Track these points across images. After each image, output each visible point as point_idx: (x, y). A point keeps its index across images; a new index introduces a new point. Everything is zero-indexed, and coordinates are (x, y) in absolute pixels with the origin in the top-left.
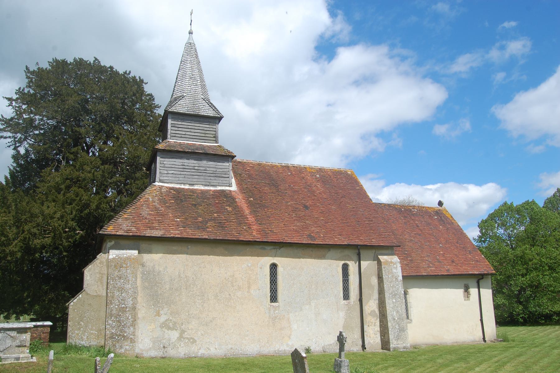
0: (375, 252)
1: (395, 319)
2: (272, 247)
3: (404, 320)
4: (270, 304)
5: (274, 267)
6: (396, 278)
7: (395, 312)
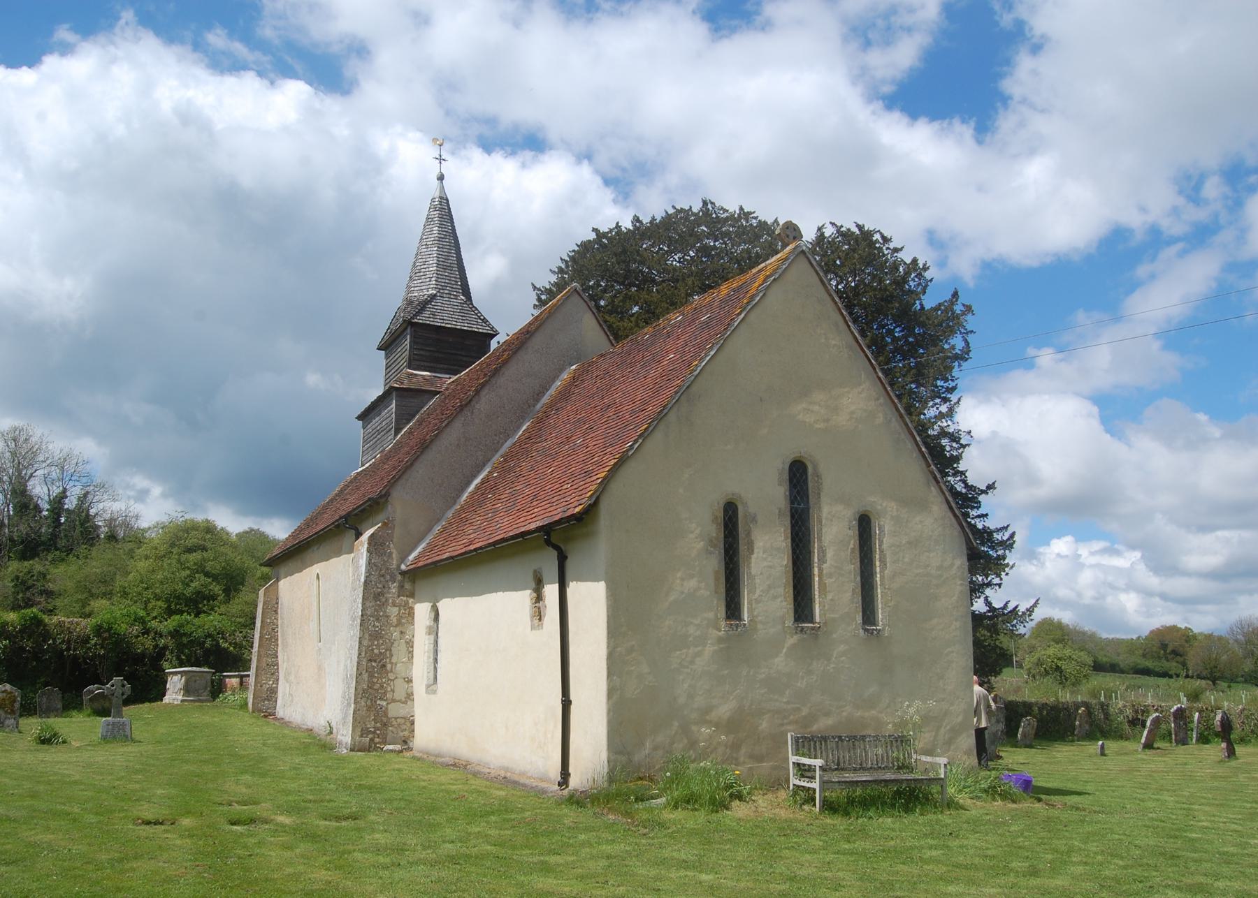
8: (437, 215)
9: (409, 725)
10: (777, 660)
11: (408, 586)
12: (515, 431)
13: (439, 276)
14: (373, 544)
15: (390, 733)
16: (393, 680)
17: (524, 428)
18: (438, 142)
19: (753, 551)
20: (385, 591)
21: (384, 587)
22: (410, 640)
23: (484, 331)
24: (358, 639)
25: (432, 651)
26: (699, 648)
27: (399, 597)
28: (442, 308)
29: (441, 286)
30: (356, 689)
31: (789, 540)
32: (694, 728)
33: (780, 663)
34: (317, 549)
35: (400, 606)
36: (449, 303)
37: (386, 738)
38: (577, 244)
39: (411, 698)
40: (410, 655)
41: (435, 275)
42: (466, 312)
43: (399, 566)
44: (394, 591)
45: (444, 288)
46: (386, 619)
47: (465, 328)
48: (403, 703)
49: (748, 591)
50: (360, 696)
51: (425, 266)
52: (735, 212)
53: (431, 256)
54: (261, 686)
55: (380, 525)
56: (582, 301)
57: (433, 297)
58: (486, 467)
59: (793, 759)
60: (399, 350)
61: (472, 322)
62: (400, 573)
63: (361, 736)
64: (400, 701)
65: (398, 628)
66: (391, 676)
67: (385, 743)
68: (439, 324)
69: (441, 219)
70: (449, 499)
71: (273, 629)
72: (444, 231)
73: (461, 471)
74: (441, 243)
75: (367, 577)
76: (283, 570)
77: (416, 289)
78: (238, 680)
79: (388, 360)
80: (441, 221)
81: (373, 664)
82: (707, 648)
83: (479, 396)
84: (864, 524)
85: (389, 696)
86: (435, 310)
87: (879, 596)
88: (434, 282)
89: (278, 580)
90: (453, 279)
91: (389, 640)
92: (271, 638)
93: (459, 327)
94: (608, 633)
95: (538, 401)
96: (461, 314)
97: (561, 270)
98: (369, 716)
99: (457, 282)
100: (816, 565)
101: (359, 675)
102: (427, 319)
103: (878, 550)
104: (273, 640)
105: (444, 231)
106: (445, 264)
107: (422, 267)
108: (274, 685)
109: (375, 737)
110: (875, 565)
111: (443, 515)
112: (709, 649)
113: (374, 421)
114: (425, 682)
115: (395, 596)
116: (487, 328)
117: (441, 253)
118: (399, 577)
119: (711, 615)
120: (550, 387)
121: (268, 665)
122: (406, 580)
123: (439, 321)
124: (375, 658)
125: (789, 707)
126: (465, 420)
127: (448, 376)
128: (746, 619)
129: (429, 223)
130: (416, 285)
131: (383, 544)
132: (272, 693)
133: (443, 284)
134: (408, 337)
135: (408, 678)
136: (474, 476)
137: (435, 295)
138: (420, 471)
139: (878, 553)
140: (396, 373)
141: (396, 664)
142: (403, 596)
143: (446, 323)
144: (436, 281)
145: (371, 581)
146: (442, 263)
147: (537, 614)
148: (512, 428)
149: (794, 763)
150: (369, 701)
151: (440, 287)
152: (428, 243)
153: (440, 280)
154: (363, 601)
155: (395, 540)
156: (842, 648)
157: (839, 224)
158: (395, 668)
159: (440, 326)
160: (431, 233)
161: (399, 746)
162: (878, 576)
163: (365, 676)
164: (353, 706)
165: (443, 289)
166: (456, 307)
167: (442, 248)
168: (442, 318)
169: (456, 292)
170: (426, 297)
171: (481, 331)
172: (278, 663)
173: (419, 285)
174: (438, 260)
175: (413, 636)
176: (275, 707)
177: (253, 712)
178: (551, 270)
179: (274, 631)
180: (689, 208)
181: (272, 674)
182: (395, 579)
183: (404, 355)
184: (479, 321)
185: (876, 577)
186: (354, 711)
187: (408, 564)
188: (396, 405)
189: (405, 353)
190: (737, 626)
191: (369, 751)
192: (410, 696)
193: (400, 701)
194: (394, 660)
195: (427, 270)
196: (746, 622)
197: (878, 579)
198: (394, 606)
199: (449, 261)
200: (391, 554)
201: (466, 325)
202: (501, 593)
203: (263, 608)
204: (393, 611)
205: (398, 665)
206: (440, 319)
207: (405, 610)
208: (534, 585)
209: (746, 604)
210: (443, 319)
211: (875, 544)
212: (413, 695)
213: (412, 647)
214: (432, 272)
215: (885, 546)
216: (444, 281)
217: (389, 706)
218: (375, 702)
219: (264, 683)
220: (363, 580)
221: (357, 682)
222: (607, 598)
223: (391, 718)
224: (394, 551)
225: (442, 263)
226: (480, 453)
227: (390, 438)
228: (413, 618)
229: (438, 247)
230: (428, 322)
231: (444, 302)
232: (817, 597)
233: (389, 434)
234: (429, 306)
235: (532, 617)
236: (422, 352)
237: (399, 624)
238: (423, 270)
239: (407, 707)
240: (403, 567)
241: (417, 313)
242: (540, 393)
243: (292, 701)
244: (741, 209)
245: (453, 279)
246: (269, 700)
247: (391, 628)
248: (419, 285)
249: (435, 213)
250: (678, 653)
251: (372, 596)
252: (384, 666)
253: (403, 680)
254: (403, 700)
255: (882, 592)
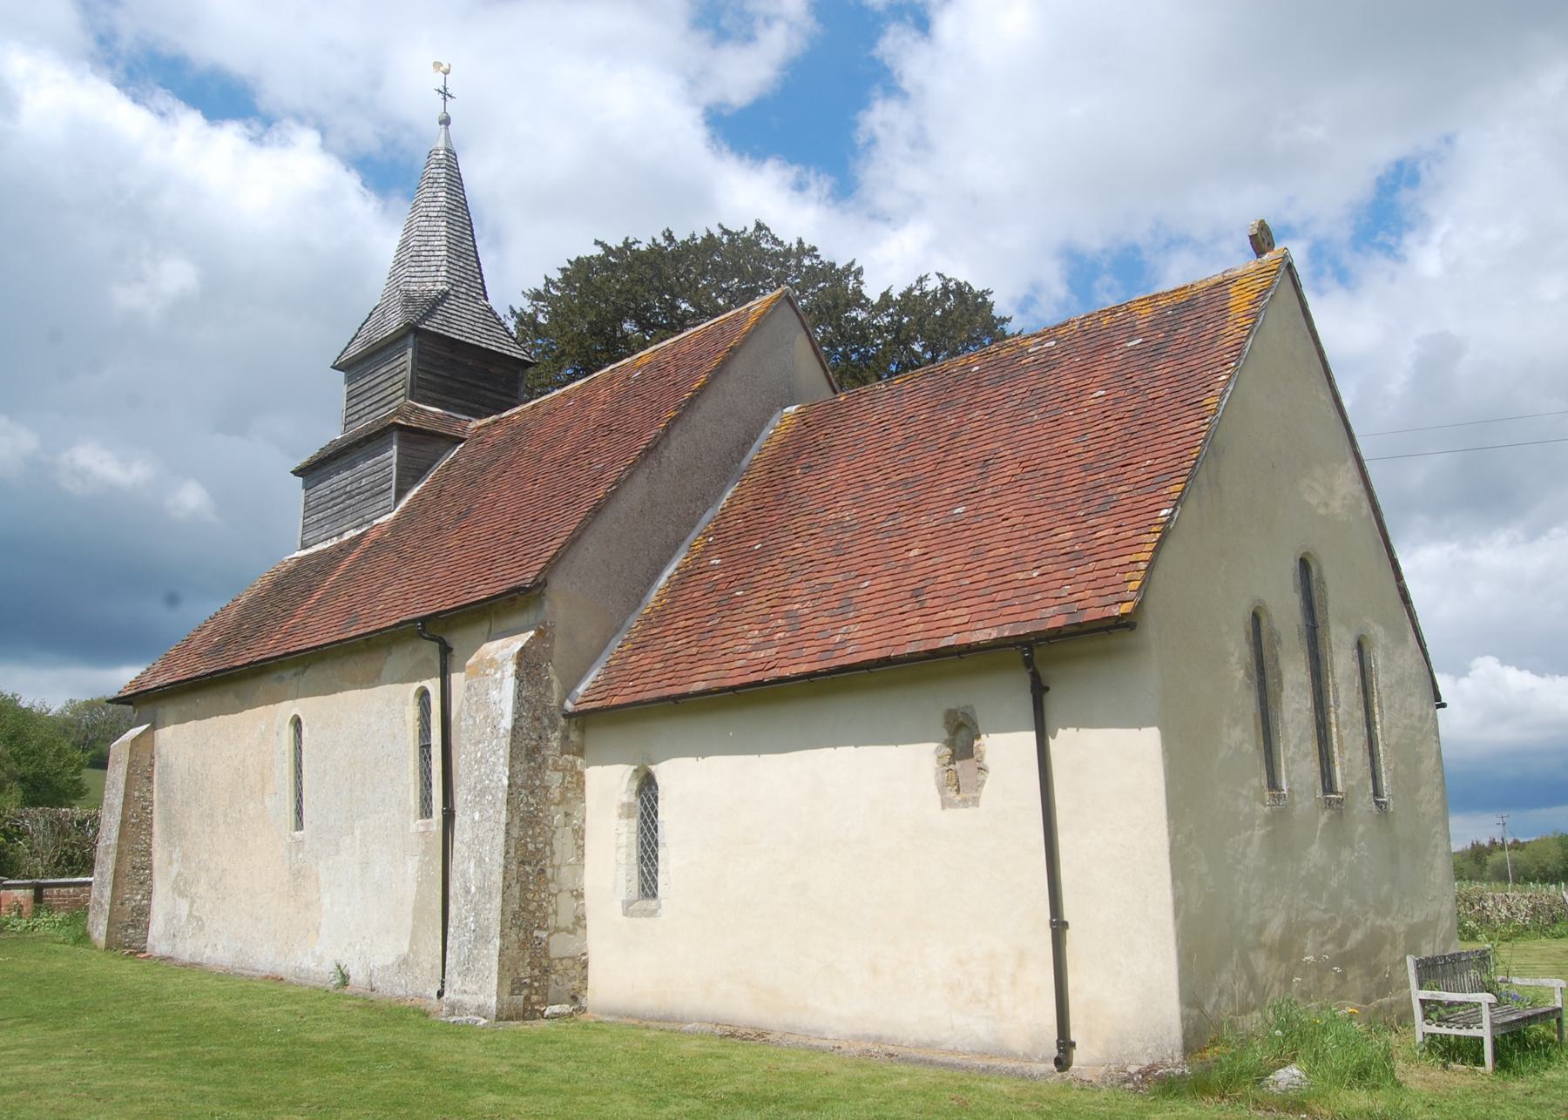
0: (490, 629)
1: (468, 892)
2: (293, 671)
3: (493, 895)
4: (293, 833)
5: (297, 723)
6: (495, 723)
7: (472, 865)
8: (444, 175)
9: (579, 969)
10: (1315, 847)
11: (574, 737)
12: (716, 498)
13: (451, 266)
14: (524, 664)
15: (554, 985)
16: (556, 895)
17: (729, 494)
18: (442, 69)
19: (1282, 687)
20: (542, 744)
21: (540, 738)
22: (580, 827)
23: (519, 357)
24: (503, 827)
25: (635, 843)
26: (1249, 833)
27: (562, 754)
28: (459, 314)
29: (455, 280)
30: (503, 913)
31: (1309, 673)
32: (1252, 956)
33: (1316, 853)
34: (295, 675)
35: (564, 770)
36: (467, 307)
37: (546, 994)
38: (569, 261)
39: (582, 923)
40: (580, 852)
41: (445, 263)
42: (491, 324)
43: (562, 704)
44: (555, 744)
45: (459, 284)
46: (544, 792)
47: (493, 348)
48: (570, 932)
49: (1284, 746)
50: (509, 924)
51: (428, 248)
52: (791, 245)
53: (437, 234)
54: (122, 904)
55: (532, 633)
56: (794, 314)
57: (446, 294)
58: (680, 550)
59: (1418, 995)
60: (383, 370)
61: (502, 341)
62: (565, 716)
63: (512, 993)
64: (566, 930)
65: (561, 807)
66: (553, 888)
67: (546, 1002)
68: (457, 337)
69: (449, 182)
70: (630, 596)
71: (144, 808)
72: (454, 200)
73: (646, 553)
74: (451, 216)
75: (515, 720)
76: (169, 709)
77: (413, 279)
78: (29, 892)
79: (354, 386)
80: (450, 185)
81: (528, 868)
82: (1256, 832)
83: (668, 438)
84: (1360, 646)
85: (551, 922)
86: (449, 315)
87: (1381, 755)
88: (444, 273)
89: (154, 727)
90: (470, 273)
91: (549, 827)
92: (137, 824)
93: (484, 346)
94: (1169, 810)
95: (743, 454)
96: (485, 327)
97: (537, 296)
98: (522, 959)
99: (476, 278)
100: (1332, 709)
101: (507, 887)
102: (440, 327)
103: (1375, 691)
104: (144, 826)
105: (454, 200)
106: (459, 249)
107: (422, 248)
108: (145, 902)
109: (531, 994)
110: (1374, 711)
111: (623, 623)
112: (1259, 833)
113: (336, 478)
114: (622, 895)
115: (558, 753)
116: (522, 352)
117: (452, 232)
118: (562, 722)
119: (1255, 782)
120: (758, 435)
121: (134, 868)
122: (573, 727)
123: (456, 331)
124: (528, 859)
125: (1326, 917)
126: (650, 473)
127: (467, 418)
128: (1284, 787)
129: (430, 185)
130: (413, 274)
131: (537, 666)
132: (141, 915)
133: (457, 278)
134: (410, 351)
135: (577, 890)
136: (664, 563)
137: (447, 293)
138: (590, 549)
139: (1376, 694)
140: (373, 407)
141: (559, 868)
142: (568, 754)
143: (467, 337)
144: (447, 271)
145: (522, 728)
146: (455, 247)
147: (954, 781)
148: (712, 492)
149: (1420, 1000)
150: (522, 932)
151: (455, 283)
152: (430, 214)
153: (452, 271)
154: (510, 761)
155: (555, 660)
156: (1361, 829)
157: (948, 277)
158: (557, 875)
159: (459, 340)
160: (435, 199)
161: (567, 1006)
162: (1378, 727)
163: (516, 890)
164: (498, 942)
165: (457, 286)
166: (477, 315)
167: (453, 224)
168: (460, 328)
169: (476, 292)
170: (434, 294)
171: (514, 355)
172: (151, 864)
173: (418, 274)
174: (447, 241)
175: (584, 820)
176: (146, 938)
177: (108, 947)
178: (523, 293)
179: (147, 810)
180: (743, 229)
181: (141, 883)
182: (557, 725)
183: (396, 379)
184: (510, 340)
185: (1376, 728)
186: (501, 950)
187: (578, 701)
188: (399, 454)
189: (401, 376)
190: (1279, 797)
191: (524, 1019)
192: (580, 921)
193: (566, 930)
194: (556, 862)
195: (431, 253)
196: (1285, 792)
197: (1378, 732)
198: (556, 770)
199: (463, 246)
200: (549, 682)
201: (493, 343)
202: (852, 748)
203: (128, 772)
204: (554, 779)
205: (564, 870)
206: (457, 329)
207: (572, 777)
208: (945, 735)
209: (1283, 764)
210: (462, 331)
211: (1372, 682)
212: (585, 919)
213: (583, 839)
214: (441, 258)
215: (1380, 685)
216: (458, 273)
217: (552, 940)
218: (531, 933)
219: (127, 899)
220: (507, 723)
221: (504, 900)
222: (1163, 753)
223: (555, 959)
224: (554, 677)
225: (455, 247)
226: (671, 527)
227: (381, 504)
228: (583, 790)
229: (448, 222)
230: (441, 332)
231: (461, 305)
232: (1336, 755)
233: (381, 497)
234: (441, 308)
235: (942, 789)
236: (429, 377)
237: (563, 799)
238: (423, 253)
239: (576, 939)
240: (569, 706)
241: (424, 314)
242: (746, 443)
243: (202, 928)
244: (800, 242)
245: (470, 273)
246: (135, 927)
247: (552, 808)
248: (418, 274)
249: (440, 171)
250: (1231, 840)
251: (524, 752)
252: (543, 871)
253: (569, 895)
254: (571, 927)
255: (1384, 750)
